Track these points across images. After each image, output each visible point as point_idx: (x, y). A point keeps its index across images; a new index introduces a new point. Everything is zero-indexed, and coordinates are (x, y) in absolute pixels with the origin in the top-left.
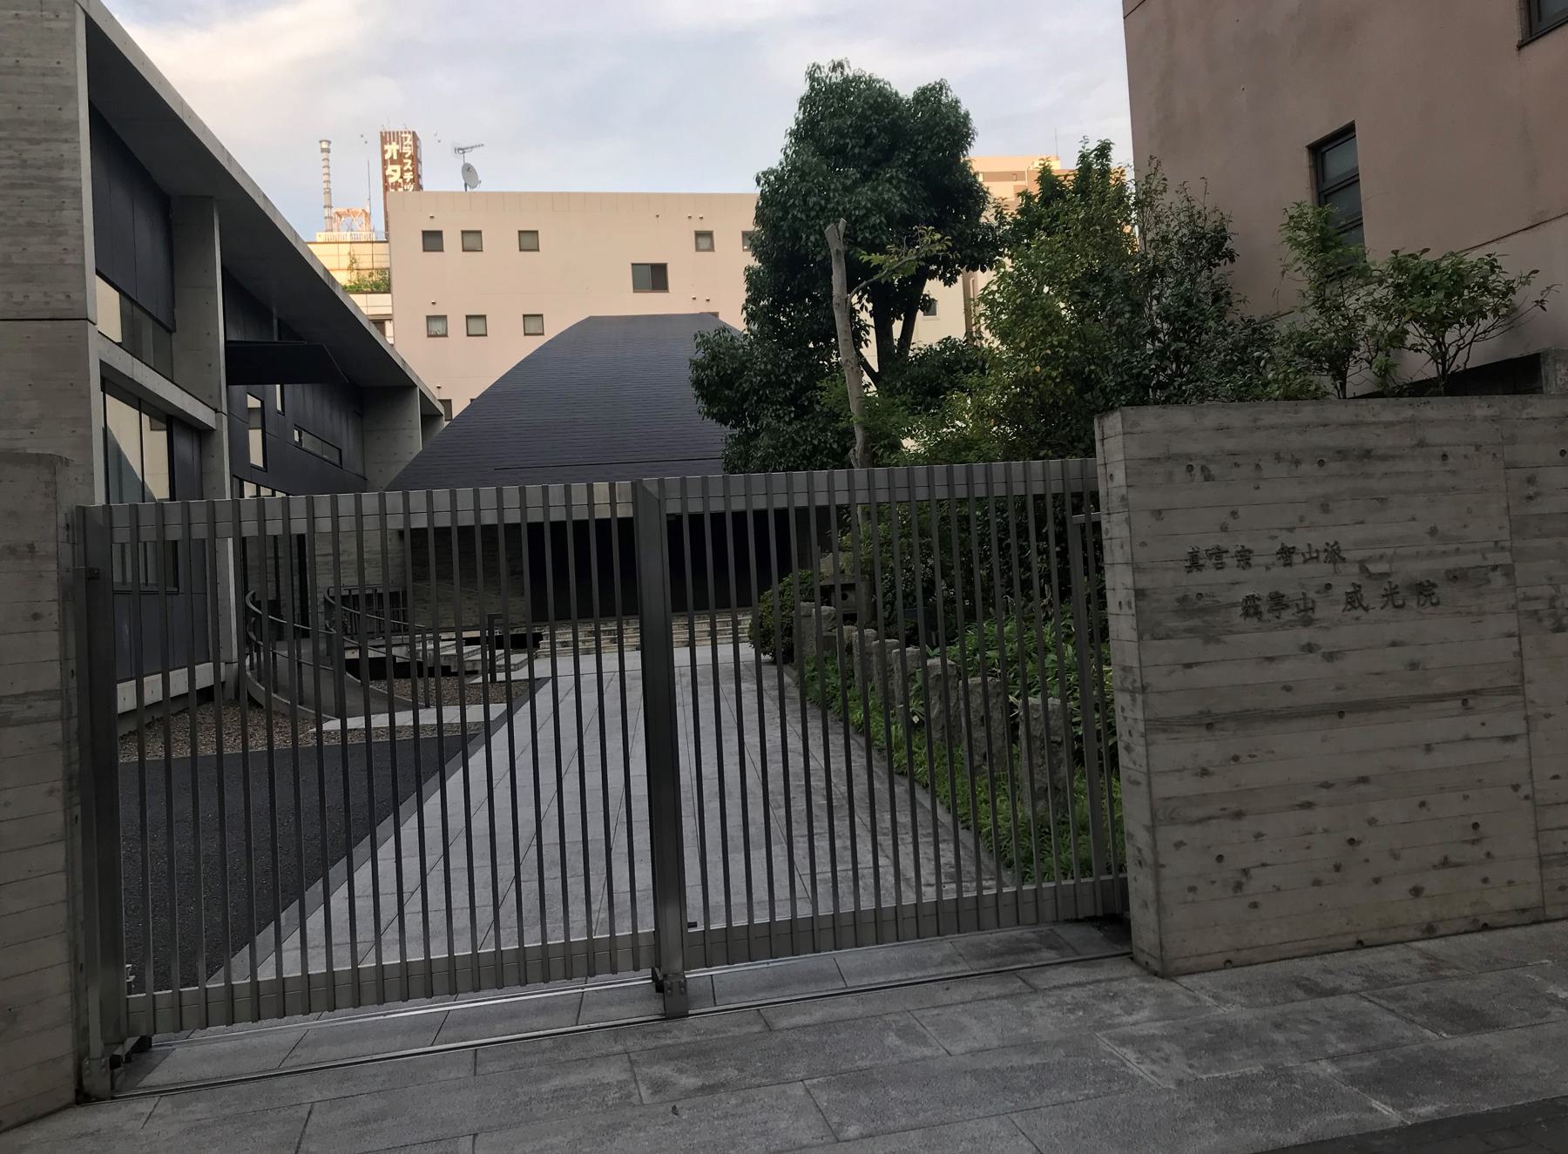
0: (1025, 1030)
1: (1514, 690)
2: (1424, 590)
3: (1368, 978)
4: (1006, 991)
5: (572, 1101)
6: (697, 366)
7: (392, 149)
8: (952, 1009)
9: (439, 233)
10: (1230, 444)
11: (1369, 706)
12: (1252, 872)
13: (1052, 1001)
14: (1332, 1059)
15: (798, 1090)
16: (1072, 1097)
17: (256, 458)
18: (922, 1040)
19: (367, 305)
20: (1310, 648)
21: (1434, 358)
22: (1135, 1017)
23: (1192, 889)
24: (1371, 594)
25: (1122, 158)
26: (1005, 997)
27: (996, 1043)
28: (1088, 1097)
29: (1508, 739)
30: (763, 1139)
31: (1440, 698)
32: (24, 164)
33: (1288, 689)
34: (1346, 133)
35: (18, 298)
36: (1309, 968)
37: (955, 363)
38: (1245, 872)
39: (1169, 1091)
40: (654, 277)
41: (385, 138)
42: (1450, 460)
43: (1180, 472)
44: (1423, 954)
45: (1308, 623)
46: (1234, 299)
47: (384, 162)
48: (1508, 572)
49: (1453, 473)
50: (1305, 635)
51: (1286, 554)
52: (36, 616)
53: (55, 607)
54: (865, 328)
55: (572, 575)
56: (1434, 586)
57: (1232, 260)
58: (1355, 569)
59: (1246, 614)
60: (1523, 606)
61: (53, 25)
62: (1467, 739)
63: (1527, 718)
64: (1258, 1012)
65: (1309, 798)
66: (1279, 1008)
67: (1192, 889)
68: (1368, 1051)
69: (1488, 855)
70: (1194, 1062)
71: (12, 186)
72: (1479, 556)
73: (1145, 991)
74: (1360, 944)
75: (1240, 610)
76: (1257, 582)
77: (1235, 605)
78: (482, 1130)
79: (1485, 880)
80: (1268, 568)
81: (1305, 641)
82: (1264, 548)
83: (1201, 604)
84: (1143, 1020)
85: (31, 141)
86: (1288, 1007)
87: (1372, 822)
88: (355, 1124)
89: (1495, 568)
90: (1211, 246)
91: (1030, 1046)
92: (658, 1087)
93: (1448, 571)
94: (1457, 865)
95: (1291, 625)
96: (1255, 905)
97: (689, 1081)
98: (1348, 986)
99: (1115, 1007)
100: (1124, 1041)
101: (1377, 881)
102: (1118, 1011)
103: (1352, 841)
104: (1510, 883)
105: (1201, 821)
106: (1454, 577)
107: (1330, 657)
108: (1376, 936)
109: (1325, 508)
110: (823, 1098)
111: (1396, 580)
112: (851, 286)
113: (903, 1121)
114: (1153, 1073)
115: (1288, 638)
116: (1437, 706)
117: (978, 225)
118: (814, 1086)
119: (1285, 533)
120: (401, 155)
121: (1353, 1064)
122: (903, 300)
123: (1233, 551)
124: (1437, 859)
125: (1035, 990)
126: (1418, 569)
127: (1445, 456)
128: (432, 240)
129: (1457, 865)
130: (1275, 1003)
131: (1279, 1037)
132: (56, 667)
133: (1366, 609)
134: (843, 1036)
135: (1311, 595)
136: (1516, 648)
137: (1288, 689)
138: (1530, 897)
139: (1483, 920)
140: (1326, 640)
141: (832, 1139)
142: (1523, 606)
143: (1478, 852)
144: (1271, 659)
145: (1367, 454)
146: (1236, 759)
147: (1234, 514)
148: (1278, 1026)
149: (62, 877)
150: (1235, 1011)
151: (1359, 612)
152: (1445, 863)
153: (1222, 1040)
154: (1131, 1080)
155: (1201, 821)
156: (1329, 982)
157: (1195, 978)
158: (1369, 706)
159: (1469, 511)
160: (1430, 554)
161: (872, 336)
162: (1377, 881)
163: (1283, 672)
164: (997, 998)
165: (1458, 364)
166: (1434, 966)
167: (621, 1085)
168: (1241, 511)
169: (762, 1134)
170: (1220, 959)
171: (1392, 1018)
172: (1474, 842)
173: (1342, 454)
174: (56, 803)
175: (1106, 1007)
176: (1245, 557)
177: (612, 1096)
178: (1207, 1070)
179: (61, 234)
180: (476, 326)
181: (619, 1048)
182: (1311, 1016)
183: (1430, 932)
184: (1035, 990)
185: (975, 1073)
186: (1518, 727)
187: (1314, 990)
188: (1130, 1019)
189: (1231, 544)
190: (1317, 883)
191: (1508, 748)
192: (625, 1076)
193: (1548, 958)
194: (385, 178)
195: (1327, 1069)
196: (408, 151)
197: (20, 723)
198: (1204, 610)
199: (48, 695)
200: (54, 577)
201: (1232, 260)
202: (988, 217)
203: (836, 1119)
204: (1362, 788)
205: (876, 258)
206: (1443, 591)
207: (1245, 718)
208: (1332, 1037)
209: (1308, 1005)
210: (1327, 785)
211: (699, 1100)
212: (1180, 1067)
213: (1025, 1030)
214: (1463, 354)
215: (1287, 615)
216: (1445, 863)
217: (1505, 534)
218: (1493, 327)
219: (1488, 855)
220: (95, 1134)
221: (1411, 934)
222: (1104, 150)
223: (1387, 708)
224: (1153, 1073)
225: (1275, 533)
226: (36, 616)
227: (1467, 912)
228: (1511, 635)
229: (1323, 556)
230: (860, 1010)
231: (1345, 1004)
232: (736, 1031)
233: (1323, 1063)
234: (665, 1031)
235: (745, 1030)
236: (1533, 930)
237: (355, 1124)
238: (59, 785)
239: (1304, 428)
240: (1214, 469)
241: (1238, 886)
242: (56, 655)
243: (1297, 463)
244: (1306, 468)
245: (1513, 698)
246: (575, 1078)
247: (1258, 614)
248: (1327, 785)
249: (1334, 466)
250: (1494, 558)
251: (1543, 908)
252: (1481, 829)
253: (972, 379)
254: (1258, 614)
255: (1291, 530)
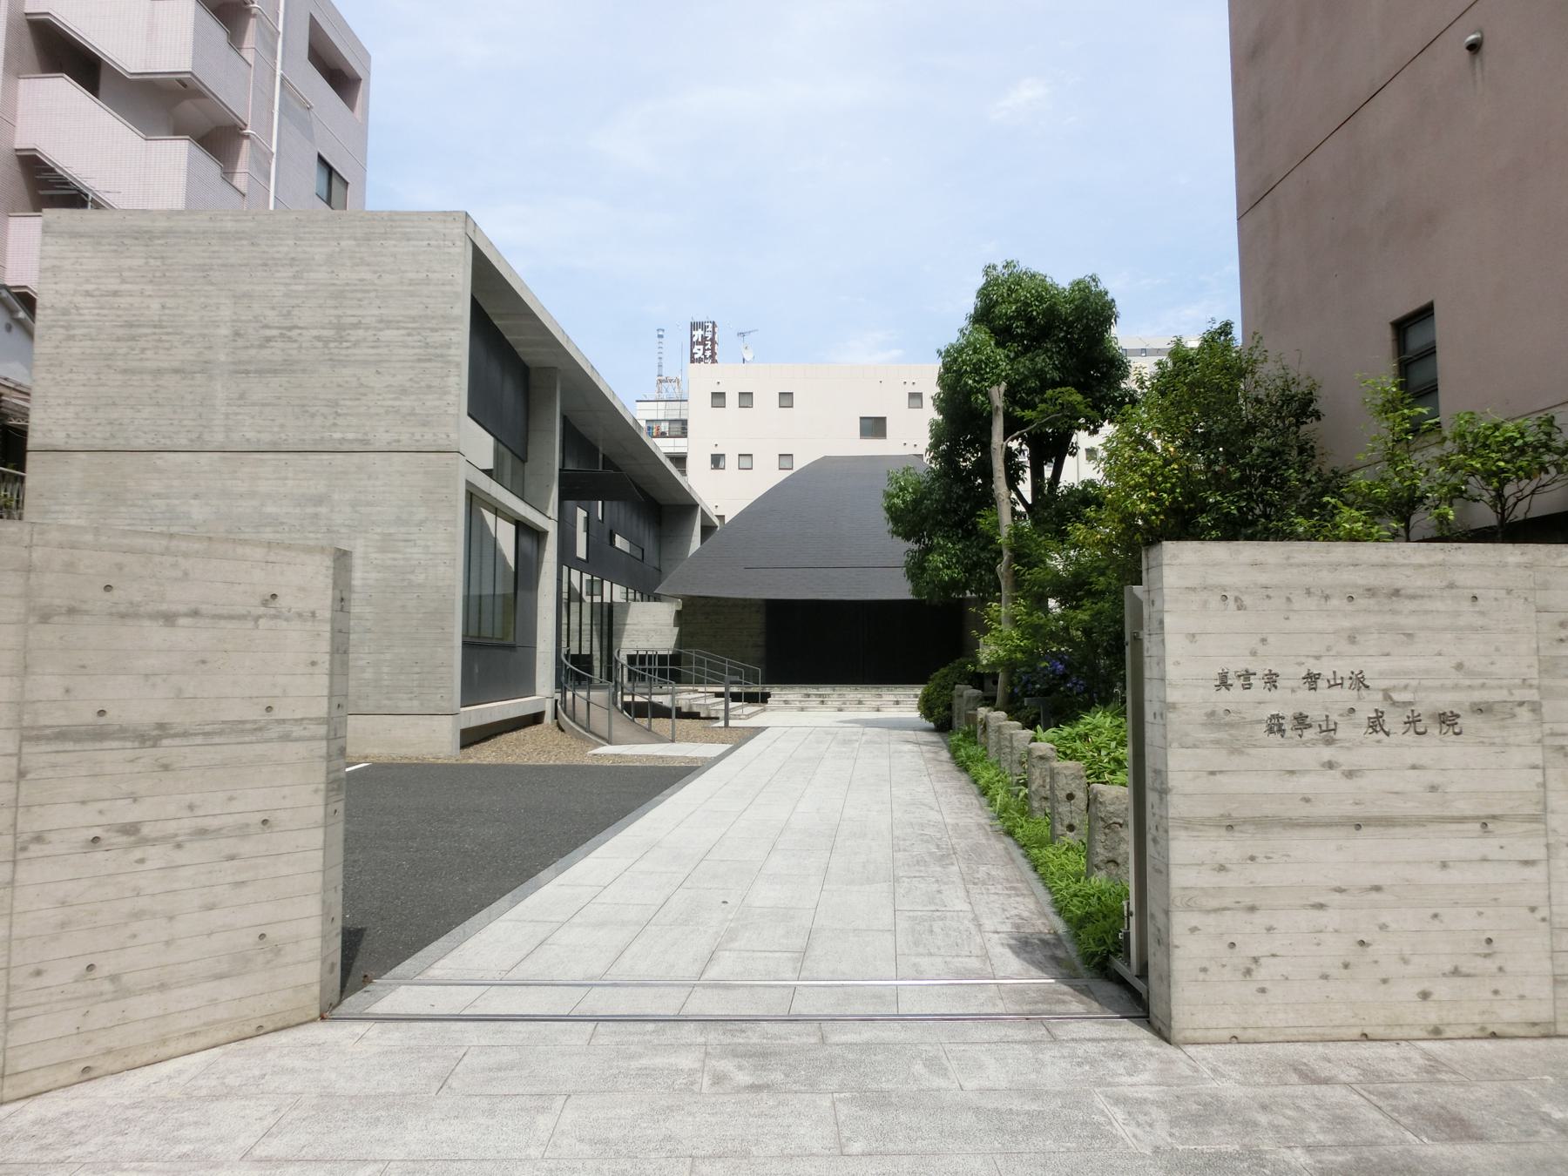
0: (1033, 1076)
1: (1533, 819)
2: (1447, 720)
3: (1365, 1072)
4: (1030, 1037)
5: (650, 1080)
6: (889, 496)
7: (698, 334)
8: (977, 1047)
9: (723, 394)
10: (1263, 579)
11: (1387, 822)
12: (1262, 961)
13: (1066, 1052)
14: (1309, 1148)
15: (826, 1102)
16: (1054, 1148)
17: (581, 552)
18: (943, 1072)
19: (664, 447)
20: (1330, 765)
21: (1494, 507)
22: (1135, 1079)
23: (1204, 970)
24: (1393, 721)
25: (1237, 332)
26: (1025, 1042)
27: (1004, 1084)
28: (1068, 1150)
29: (1527, 863)
30: (780, 1142)
31: (1462, 819)
32: (427, 345)
33: (1307, 800)
34: (1426, 312)
35: (418, 437)
36: (1309, 1054)
37: (1086, 497)
38: (1256, 960)
39: (1144, 1157)
40: (874, 427)
41: (694, 326)
42: (1480, 601)
43: (1214, 601)
44: (1426, 1055)
45: (1329, 742)
46: (1317, 452)
47: (693, 344)
48: (1536, 708)
49: (1482, 613)
50: (1327, 753)
51: (1312, 679)
52: (313, 664)
53: (327, 657)
54: (1022, 467)
55: (807, 643)
56: (1458, 716)
57: (1318, 418)
58: (1380, 696)
59: (1271, 731)
60: (1548, 741)
61: (452, 250)
62: (1485, 860)
63: (1548, 846)
64: (1250, 1091)
65: (1321, 900)
66: (1270, 1090)
67: (1204, 970)
68: (1345, 1145)
69: (1501, 969)
70: (1176, 1131)
71: (419, 360)
72: (1505, 692)
73: (1151, 1054)
74: (1365, 1037)
75: (1264, 727)
76: (1284, 702)
77: (1260, 722)
78: (575, 1092)
79: (1496, 992)
80: (1293, 691)
81: (1326, 759)
82: (1292, 674)
83: (1227, 719)
84: (1141, 1084)
85: (433, 330)
86: (1280, 1089)
87: (1383, 927)
88: (490, 1070)
89: (1521, 704)
90: (1302, 407)
91: (1037, 1094)
92: (719, 1079)
93: (1473, 704)
94: (1468, 976)
95: (1314, 743)
96: (1263, 991)
97: (743, 1078)
98: (1343, 1077)
99: (1119, 1067)
100: (1118, 1101)
101: (1385, 981)
102: (1122, 1071)
103: (1362, 943)
104: (1522, 997)
105: (1216, 910)
106: (1480, 709)
107: (1350, 774)
108: (1380, 1032)
109: (1352, 640)
110: (843, 1111)
111: (1419, 709)
112: (1008, 433)
113: (902, 1146)
114: (1135, 1136)
115: (1309, 754)
116: (1454, 827)
117: (1119, 389)
118: (840, 1100)
119: (1312, 661)
120: (704, 338)
121: (1328, 1157)
122: (1053, 448)
123: (1260, 674)
124: (1448, 967)
125: (1055, 1039)
126: (1445, 701)
127: (1475, 598)
128: (718, 398)
129: (1468, 976)
130: (1267, 1084)
131: (1263, 1119)
132: (325, 702)
133: (1387, 734)
134: (879, 1058)
135: (1334, 717)
136: (1540, 779)
137: (1307, 800)
138: (1543, 1012)
139: (1491, 1029)
140: (1345, 759)
141: (837, 1152)
142: (1548, 741)
143: (1491, 965)
144: (1292, 772)
145: (1396, 593)
146: (1252, 858)
147: (1264, 641)
148: (1264, 1107)
149: (321, 853)
150: (1230, 1089)
151: (1381, 735)
152: (1456, 972)
153: (1210, 1112)
154: (1113, 1139)
155: (1216, 910)
156: (1325, 1070)
157: (1200, 1048)
158: (1387, 822)
159: (1497, 649)
160: (1456, 687)
161: (1028, 475)
162: (1385, 981)
163: (1304, 784)
164: (1019, 1042)
165: (1519, 513)
166: (1434, 1067)
167: (692, 1072)
168: (1271, 639)
169: (784, 1136)
170: (1226, 1035)
171: (1377, 1116)
172: (1486, 956)
173: (1371, 592)
174: (319, 799)
175: (1111, 1065)
176: (1272, 680)
177: (681, 1081)
178: (1185, 1141)
179: (446, 393)
180: (745, 462)
181: (701, 1040)
182: (1298, 1102)
183: (1436, 1033)
184: (1055, 1039)
185: (977, 1110)
186: (1538, 853)
187: (1309, 1077)
188: (1129, 1080)
189: (1260, 668)
190: (1325, 977)
191: (1528, 872)
192: (697, 1065)
193: (1552, 1075)
194: (692, 354)
195: (1300, 1158)
196: (709, 335)
197: (296, 740)
198: (1231, 725)
199: (318, 721)
200: (328, 635)
201: (1318, 418)
202: (1130, 384)
203: (847, 1133)
204: (1375, 896)
205: (1029, 414)
206: (1465, 722)
207: (1264, 823)
208: (1313, 1126)
209: (1299, 1090)
210: (1340, 890)
211: (745, 1096)
212: (1161, 1135)
213: (1033, 1076)
214: (1523, 505)
215: (1309, 734)
216: (1456, 972)
217: (1534, 673)
218: (1553, 481)
219: (1501, 969)
220: (319, 1046)
221: (1417, 1033)
222: (1226, 329)
223: (1404, 825)
224: (1135, 1136)
225: (1303, 659)
226: (313, 664)
227: (1477, 1019)
228: (1535, 767)
229: (1347, 683)
230: (902, 1036)
231: (1335, 1094)
232: (796, 1040)
233: (1298, 1152)
234: (743, 1031)
235: (804, 1040)
236: (1542, 1044)
237: (490, 1070)
238: (322, 786)
239: (1335, 567)
240: (1247, 600)
241: (1248, 972)
242: (326, 692)
243: (1327, 598)
244: (1334, 602)
245: (1535, 826)
246: (659, 1061)
247: (1281, 731)
248: (1340, 890)
249: (1362, 602)
250: (1519, 695)
251: (1554, 1023)
252: (1495, 944)
253: (1090, 512)
254: (1281, 731)
255: (1318, 658)
